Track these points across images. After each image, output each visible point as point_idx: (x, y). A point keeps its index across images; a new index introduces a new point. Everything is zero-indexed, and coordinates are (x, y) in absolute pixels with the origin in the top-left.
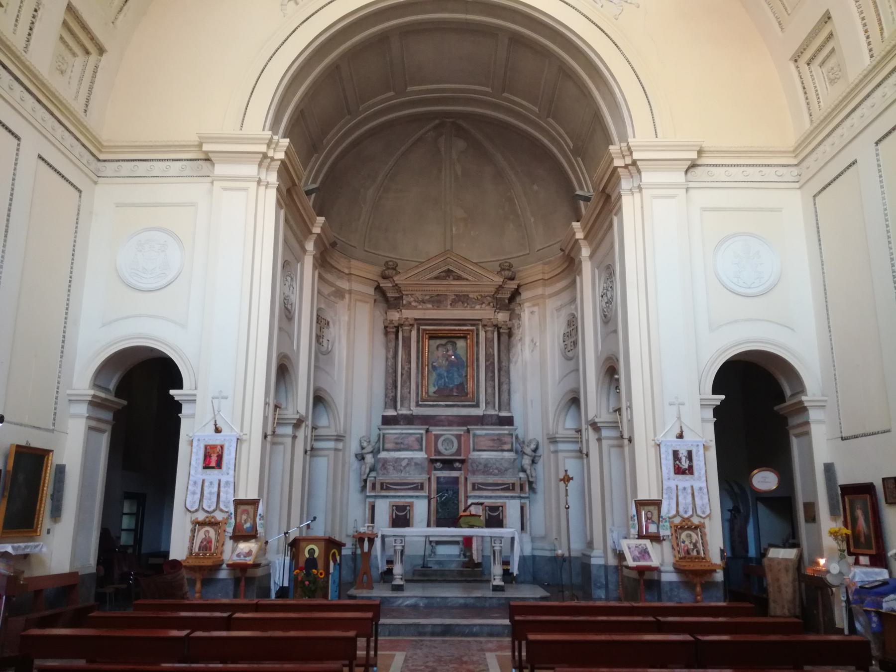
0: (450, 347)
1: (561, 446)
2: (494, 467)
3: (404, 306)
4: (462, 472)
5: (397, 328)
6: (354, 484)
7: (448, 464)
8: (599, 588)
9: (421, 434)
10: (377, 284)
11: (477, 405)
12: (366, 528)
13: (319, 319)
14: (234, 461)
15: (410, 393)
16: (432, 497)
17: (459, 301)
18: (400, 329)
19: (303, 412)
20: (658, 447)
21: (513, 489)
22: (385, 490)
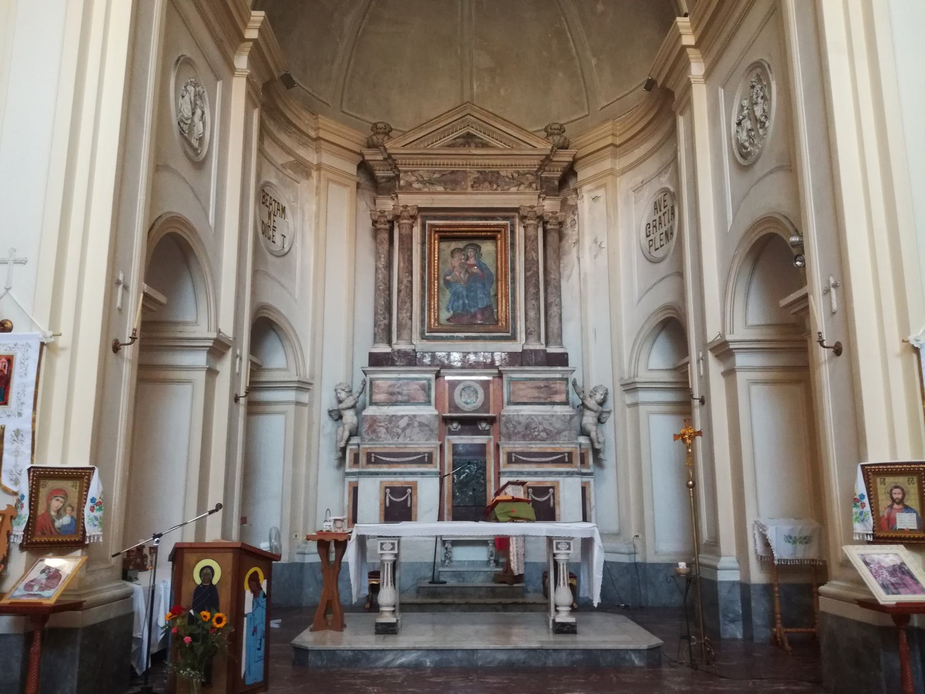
0: (470, 252)
1: (643, 396)
2: (541, 428)
3: (401, 188)
4: (491, 437)
5: (391, 222)
6: (327, 456)
7: (469, 423)
8: (733, 621)
9: (429, 380)
10: (360, 159)
11: (513, 338)
12: (331, 524)
13: (264, 196)
14: (33, 388)
15: (411, 319)
16: (446, 473)
17: (485, 180)
18: (396, 224)
19: (228, 330)
20: (915, 356)
21: (570, 461)
22: (373, 463)
